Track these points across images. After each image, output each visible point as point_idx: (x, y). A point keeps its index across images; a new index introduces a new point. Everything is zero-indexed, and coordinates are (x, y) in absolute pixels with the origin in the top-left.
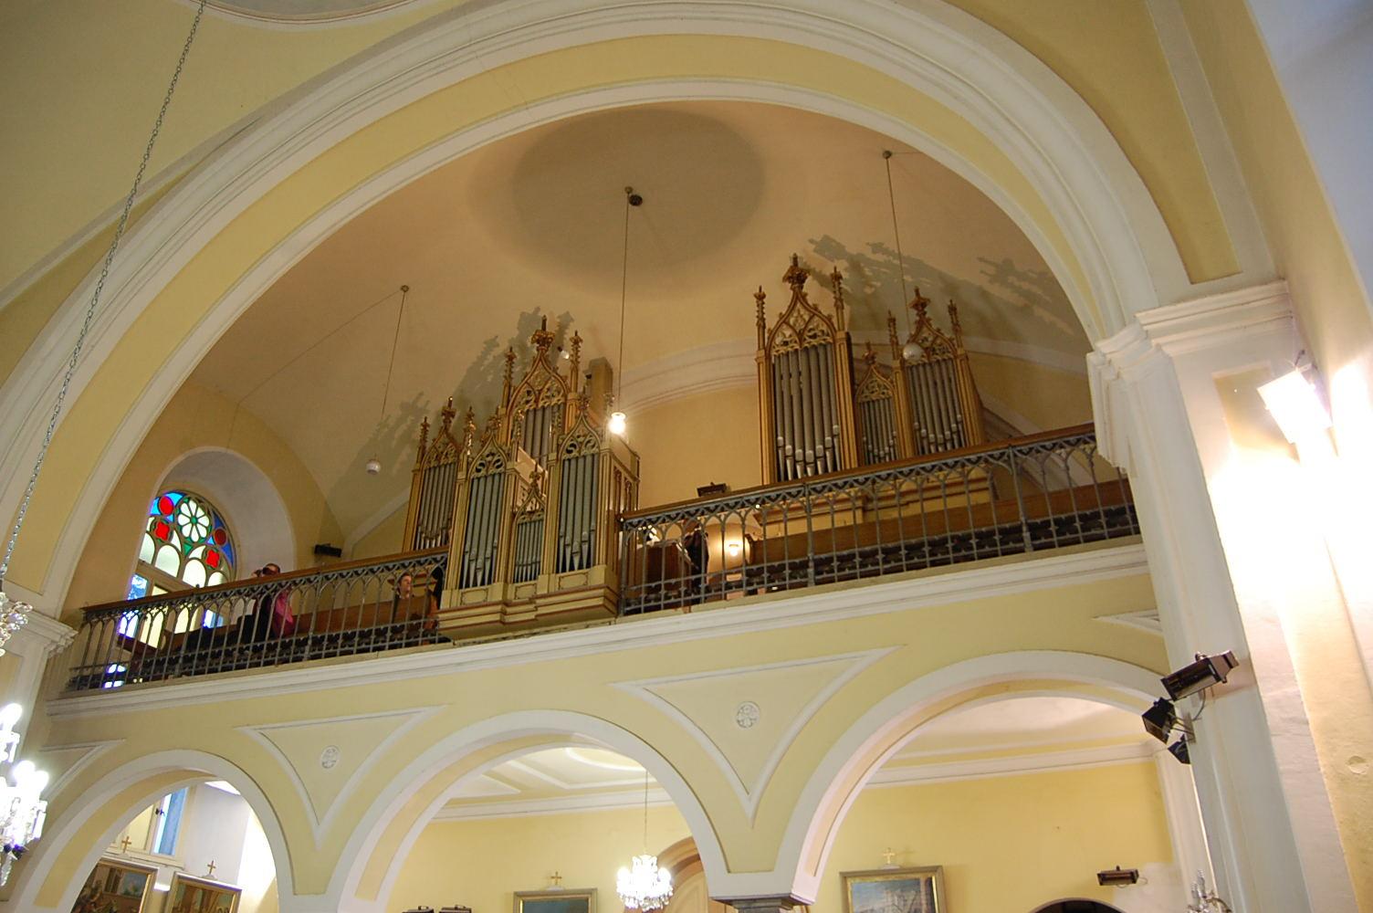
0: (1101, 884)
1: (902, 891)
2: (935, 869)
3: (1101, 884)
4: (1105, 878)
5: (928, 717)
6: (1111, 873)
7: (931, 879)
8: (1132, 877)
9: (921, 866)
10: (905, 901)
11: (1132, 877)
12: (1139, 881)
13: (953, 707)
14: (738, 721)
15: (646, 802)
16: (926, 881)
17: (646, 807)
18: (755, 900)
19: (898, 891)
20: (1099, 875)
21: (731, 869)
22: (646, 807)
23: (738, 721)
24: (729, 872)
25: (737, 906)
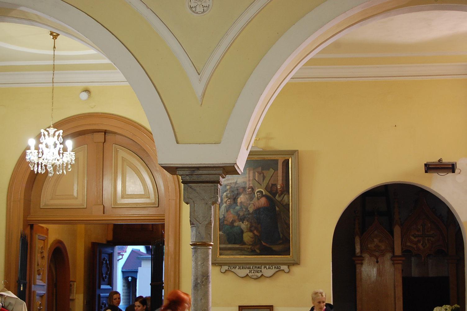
0: (426, 172)
1: (262, 170)
2: (293, 153)
3: (426, 172)
4: (430, 168)
5: (360, 19)
6: (433, 164)
7: (289, 160)
8: (451, 168)
9: (279, 149)
10: (264, 178)
11: (451, 168)
12: (457, 171)
13: (383, 12)
14: (191, 8)
15: (53, 82)
16: (283, 162)
17: (53, 87)
18: (198, 168)
19: (260, 169)
20: (426, 165)
21: (179, 139)
22: (53, 87)
23: (191, 8)
24: (178, 143)
25: (181, 173)
